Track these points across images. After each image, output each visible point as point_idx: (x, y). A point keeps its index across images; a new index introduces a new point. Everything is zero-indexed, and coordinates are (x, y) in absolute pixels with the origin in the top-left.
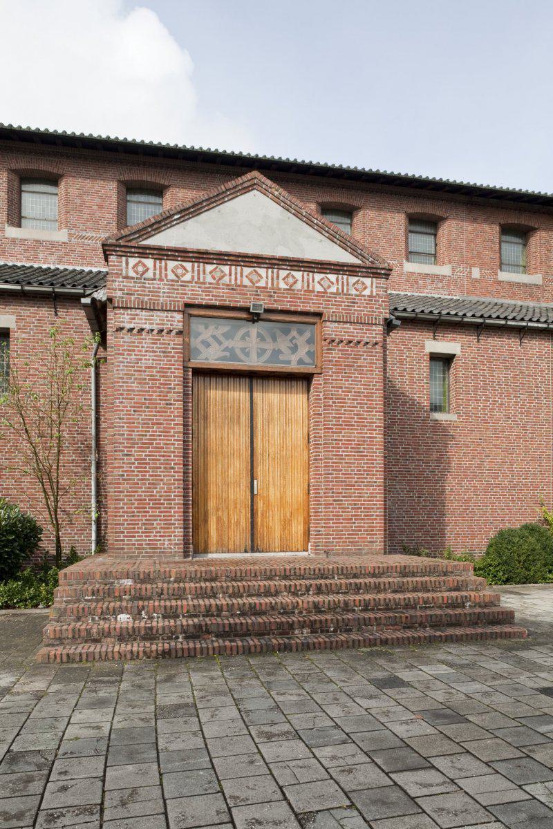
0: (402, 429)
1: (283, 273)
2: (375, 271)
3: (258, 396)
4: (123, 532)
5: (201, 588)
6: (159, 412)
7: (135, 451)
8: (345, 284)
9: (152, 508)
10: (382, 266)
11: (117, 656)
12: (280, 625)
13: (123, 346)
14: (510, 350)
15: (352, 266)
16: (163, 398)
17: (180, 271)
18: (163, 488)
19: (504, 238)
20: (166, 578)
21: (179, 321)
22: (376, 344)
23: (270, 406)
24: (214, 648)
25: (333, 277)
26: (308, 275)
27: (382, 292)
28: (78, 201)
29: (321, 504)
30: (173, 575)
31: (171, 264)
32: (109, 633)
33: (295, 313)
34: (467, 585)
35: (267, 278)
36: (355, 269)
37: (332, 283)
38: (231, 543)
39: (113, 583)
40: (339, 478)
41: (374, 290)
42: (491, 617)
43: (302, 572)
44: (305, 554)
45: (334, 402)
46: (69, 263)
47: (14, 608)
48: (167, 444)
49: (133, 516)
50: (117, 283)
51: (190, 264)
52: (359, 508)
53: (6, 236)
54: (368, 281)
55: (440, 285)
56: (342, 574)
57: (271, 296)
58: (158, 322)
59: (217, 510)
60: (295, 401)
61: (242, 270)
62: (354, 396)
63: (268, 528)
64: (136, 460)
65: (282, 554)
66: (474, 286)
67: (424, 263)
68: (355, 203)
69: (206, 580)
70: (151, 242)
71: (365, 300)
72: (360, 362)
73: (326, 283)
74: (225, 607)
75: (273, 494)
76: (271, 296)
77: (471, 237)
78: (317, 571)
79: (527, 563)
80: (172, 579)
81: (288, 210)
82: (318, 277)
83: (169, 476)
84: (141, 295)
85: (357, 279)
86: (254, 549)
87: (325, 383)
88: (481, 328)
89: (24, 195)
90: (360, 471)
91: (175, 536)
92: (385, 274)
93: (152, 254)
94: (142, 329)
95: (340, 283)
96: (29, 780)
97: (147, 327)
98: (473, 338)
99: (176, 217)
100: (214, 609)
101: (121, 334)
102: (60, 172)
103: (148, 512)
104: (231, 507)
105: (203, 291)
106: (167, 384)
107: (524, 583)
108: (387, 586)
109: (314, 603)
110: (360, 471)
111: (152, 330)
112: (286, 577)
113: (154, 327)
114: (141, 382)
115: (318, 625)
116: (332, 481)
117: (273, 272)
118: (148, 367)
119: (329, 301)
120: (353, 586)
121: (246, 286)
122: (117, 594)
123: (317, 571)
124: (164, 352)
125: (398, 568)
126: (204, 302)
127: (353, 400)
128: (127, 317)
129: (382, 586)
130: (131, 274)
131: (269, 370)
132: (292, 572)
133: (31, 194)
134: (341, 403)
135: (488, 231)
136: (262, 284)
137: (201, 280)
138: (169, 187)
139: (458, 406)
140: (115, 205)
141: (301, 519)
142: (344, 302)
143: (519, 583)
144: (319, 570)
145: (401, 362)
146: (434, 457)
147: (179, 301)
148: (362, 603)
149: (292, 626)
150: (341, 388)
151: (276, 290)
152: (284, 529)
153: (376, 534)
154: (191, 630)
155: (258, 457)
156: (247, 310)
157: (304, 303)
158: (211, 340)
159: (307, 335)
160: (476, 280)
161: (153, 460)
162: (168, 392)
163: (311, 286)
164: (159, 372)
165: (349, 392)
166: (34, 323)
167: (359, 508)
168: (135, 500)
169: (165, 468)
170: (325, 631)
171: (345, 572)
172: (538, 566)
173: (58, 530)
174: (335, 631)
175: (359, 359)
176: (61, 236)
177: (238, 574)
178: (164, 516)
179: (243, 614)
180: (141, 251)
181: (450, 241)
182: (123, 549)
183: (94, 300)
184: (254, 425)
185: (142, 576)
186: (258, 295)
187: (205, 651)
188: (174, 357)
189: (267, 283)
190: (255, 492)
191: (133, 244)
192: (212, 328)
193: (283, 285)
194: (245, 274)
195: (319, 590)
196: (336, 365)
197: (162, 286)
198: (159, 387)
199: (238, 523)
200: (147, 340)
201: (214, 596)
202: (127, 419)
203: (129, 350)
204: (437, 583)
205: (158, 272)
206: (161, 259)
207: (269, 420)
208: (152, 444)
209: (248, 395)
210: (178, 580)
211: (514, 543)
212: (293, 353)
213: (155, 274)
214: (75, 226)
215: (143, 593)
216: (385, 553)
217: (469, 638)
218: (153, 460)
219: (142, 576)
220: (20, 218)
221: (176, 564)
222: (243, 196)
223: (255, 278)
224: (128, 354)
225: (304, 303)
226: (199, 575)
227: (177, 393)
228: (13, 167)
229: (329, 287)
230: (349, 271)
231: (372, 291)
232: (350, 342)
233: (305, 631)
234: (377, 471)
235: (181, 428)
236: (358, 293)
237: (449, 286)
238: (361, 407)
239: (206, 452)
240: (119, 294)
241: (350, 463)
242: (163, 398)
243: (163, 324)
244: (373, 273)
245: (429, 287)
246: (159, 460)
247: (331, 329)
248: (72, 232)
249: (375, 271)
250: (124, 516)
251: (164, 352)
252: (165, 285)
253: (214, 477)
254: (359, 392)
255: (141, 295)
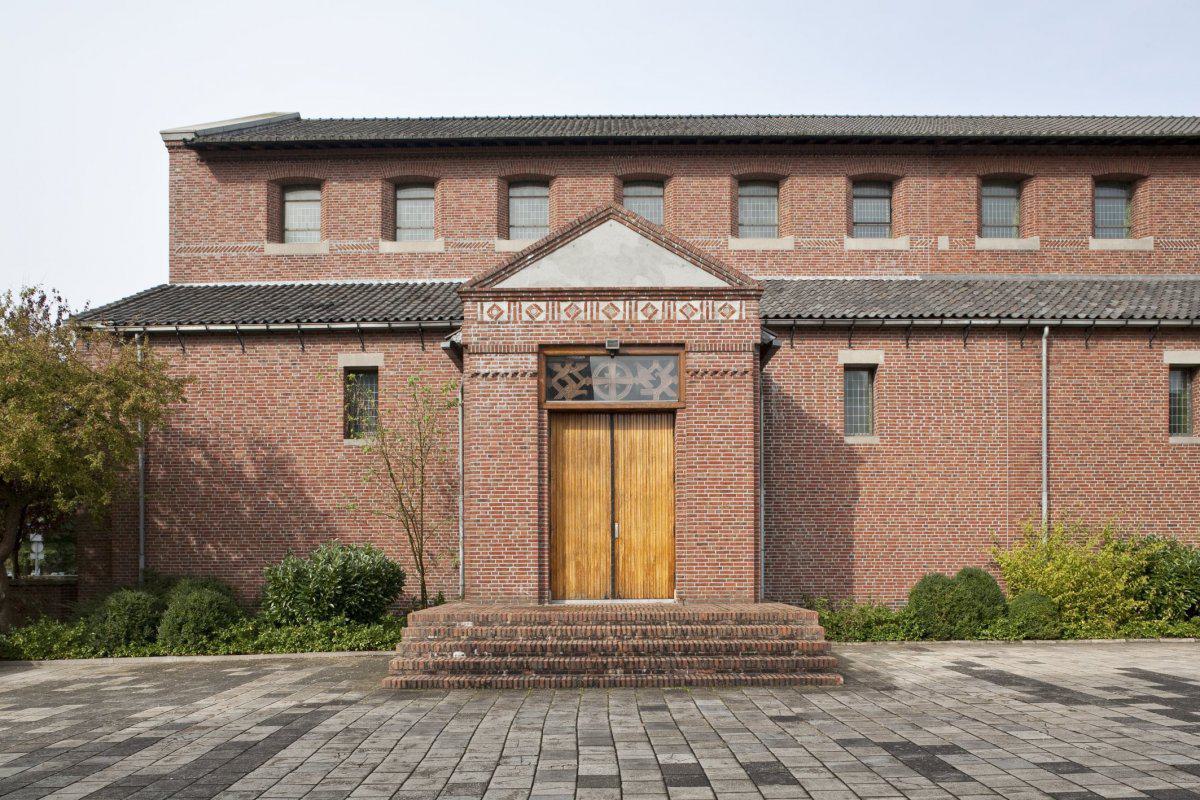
0: (809, 457)
1: (642, 304)
2: (743, 293)
3: (619, 433)
4: (478, 578)
5: (531, 631)
6: (514, 456)
7: (491, 497)
8: (710, 309)
9: (507, 553)
10: (752, 287)
11: (446, 685)
12: (595, 665)
13: (478, 392)
14: (950, 354)
15: (718, 290)
16: (518, 441)
17: (534, 312)
18: (518, 533)
19: (987, 191)
20: (502, 621)
21: (533, 363)
22: (746, 372)
23: (632, 444)
24: (529, 681)
25: (696, 304)
26: (669, 304)
27: (752, 315)
28: (455, 205)
29: (684, 548)
30: (509, 618)
31: (526, 305)
32: (443, 667)
33: (655, 345)
34: (802, 633)
35: (625, 310)
36: (721, 293)
37: (696, 310)
38: (591, 589)
39: (455, 625)
40: (704, 519)
41: (744, 313)
42: (811, 666)
43: (634, 618)
44: (670, 601)
45: (697, 439)
46: (446, 275)
47: (376, 649)
48: (522, 489)
49: (488, 561)
50: (472, 329)
51: (545, 303)
52: (725, 552)
53: (381, 251)
54: (736, 304)
55: (894, 262)
56: (675, 620)
57: (628, 330)
58: (513, 365)
59: (576, 554)
60: (661, 438)
61: (598, 304)
62: (719, 430)
63: (630, 574)
64: (491, 505)
65: (645, 601)
66: (941, 261)
67: (874, 236)
68: (780, 172)
69: (540, 624)
70: (507, 284)
71: (732, 326)
72: (728, 394)
73: (689, 311)
74: (549, 648)
75: (636, 537)
76: (628, 330)
77: (936, 196)
78: (648, 618)
79: (951, 617)
80: (508, 622)
81: (646, 237)
82: (680, 305)
83: (523, 521)
84: (495, 339)
85: (723, 303)
86: (615, 595)
87: (688, 419)
88: (909, 331)
89: (400, 204)
90: (727, 511)
91: (530, 582)
92: (755, 295)
93: (507, 297)
94: (497, 374)
95: (705, 310)
96: (356, 738)
97: (502, 371)
98: (900, 343)
99: (529, 257)
100: (539, 649)
101: (476, 380)
102: (437, 175)
103: (503, 557)
104: (591, 551)
105: (558, 330)
106: (521, 428)
107: (948, 639)
108: (715, 633)
109: (633, 646)
110: (727, 511)
111: (507, 374)
112: (617, 622)
113: (509, 370)
114: (496, 426)
115: (631, 666)
116: (695, 524)
117: (630, 304)
118: (503, 412)
119: (693, 330)
120: (679, 632)
121: (602, 322)
122: (456, 634)
123: (648, 618)
124: (518, 395)
125: (734, 616)
126: (558, 342)
127: (719, 435)
128: (482, 362)
129: (709, 633)
130: (487, 318)
131: (627, 407)
132: (624, 617)
133: (406, 202)
134: (705, 439)
135: (959, 187)
136: (619, 317)
137: (556, 318)
138: (555, 177)
139: (881, 426)
140: (494, 206)
141: (666, 564)
142: (709, 330)
143: (940, 639)
144: (651, 616)
145: (808, 378)
146: (850, 488)
147: (532, 343)
148: (682, 649)
149: (605, 666)
150: (706, 423)
151: (634, 323)
152: (648, 574)
153: (745, 581)
154: (514, 666)
155: (619, 498)
156: (602, 345)
157: (664, 334)
158: (568, 379)
159: (671, 366)
160: (945, 253)
161: (508, 505)
162: (523, 436)
163: (672, 315)
164: (513, 416)
165: (715, 427)
166: (401, 359)
167: (725, 552)
168: (491, 545)
169: (520, 513)
170: (637, 672)
171: (677, 618)
172: (966, 619)
173: (423, 575)
174: (648, 672)
175: (725, 390)
176: (437, 246)
177: (571, 619)
178: (519, 561)
179: (566, 655)
180: (495, 295)
181: (907, 206)
182: (479, 594)
183: (453, 343)
184: (615, 466)
185: (481, 620)
186: (615, 330)
187: (521, 684)
188: (528, 399)
189: (624, 315)
190: (616, 536)
191: (487, 288)
192: (568, 366)
193: (641, 317)
194: (601, 308)
195: (645, 634)
196: (700, 398)
197: (516, 328)
198: (513, 431)
199: (598, 569)
200: (501, 385)
201: (544, 638)
202: (483, 464)
203: (484, 396)
204: (769, 631)
205: (512, 314)
206: (515, 301)
207: (632, 459)
208: (507, 489)
209: (609, 432)
210: (514, 623)
211: (935, 591)
212: (655, 387)
213: (509, 317)
214: (451, 234)
215: (479, 634)
216: (756, 601)
217: (777, 683)
218: (508, 505)
219: (481, 620)
220: (395, 228)
221: (530, 606)
222: (599, 227)
223: (612, 311)
224: (483, 400)
225: (664, 334)
226: (533, 619)
227: (532, 436)
228: (388, 175)
229: (692, 314)
230: (715, 296)
231: (741, 316)
232: (716, 372)
233: (618, 671)
234: (746, 512)
235: (535, 472)
236: (724, 318)
237: (905, 263)
238: (728, 443)
239: (563, 495)
240: (475, 339)
241: (715, 504)
242: (518, 441)
243: (517, 367)
244: (742, 296)
245: (879, 267)
246: (514, 505)
247: (694, 360)
248: (449, 240)
249: (743, 293)
250: (479, 562)
251: (518, 395)
252: (520, 327)
253: (571, 521)
254: (726, 427)
255: (495, 339)
